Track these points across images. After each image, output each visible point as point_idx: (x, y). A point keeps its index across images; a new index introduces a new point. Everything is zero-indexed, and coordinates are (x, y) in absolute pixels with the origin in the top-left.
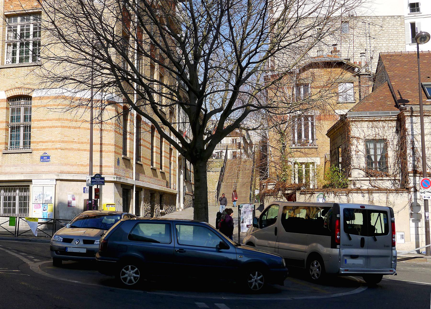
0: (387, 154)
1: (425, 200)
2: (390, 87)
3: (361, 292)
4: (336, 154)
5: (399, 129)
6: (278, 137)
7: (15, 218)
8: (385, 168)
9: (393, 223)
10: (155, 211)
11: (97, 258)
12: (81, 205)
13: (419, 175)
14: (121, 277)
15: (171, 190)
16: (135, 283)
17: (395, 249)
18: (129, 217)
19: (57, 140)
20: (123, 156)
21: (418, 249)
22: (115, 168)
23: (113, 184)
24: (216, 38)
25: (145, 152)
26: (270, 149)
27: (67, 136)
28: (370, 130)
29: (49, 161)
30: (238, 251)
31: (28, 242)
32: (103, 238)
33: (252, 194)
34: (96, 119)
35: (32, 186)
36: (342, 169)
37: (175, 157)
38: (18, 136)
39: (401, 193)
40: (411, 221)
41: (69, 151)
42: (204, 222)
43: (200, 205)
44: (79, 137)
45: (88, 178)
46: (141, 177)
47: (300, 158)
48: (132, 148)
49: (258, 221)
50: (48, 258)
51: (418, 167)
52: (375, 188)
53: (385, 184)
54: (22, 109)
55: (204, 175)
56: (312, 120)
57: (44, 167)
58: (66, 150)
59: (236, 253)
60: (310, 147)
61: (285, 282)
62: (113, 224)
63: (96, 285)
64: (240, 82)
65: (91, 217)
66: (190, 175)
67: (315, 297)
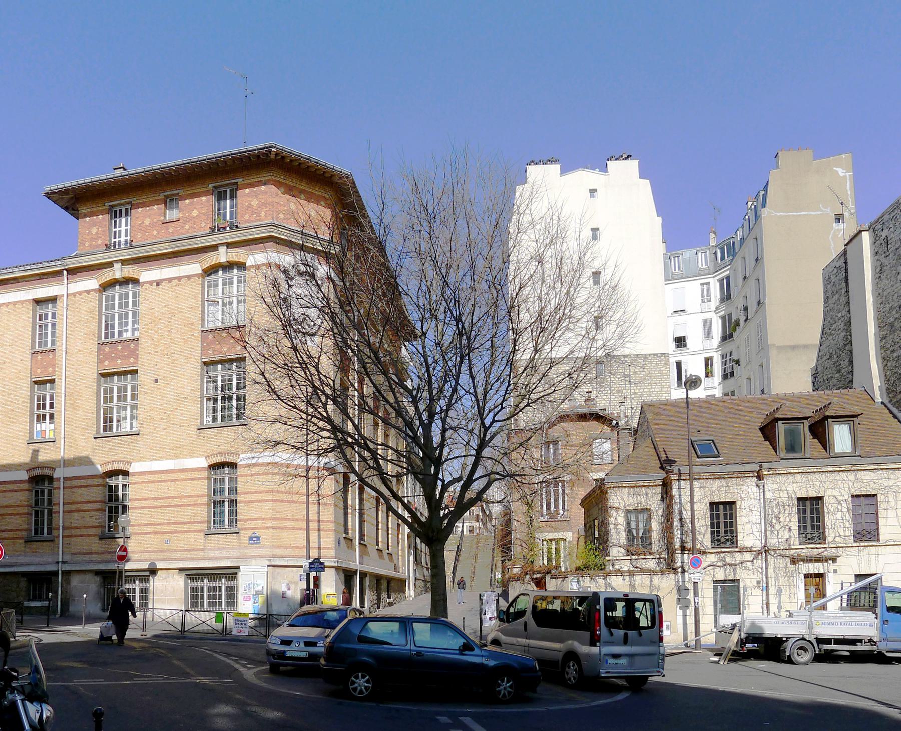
0: (651, 527)
1: (694, 583)
5: (665, 496)
6: (525, 508)
7: (222, 613)
8: (648, 545)
9: (660, 613)
11: (322, 665)
13: (687, 552)
14: (351, 687)
16: (366, 694)
21: (686, 642)
24: (455, 390)
25: (369, 529)
26: (515, 524)
27: (280, 512)
30: (484, 654)
31: (238, 643)
35: (240, 573)
37: (403, 535)
38: (222, 513)
40: (678, 608)
42: (443, 619)
45: (306, 563)
50: (262, 663)
51: (687, 543)
54: (226, 480)
56: (563, 486)
57: (253, 551)
59: (482, 656)
60: (561, 520)
61: (538, 689)
63: (321, 697)
64: (482, 445)
67: (572, 707)
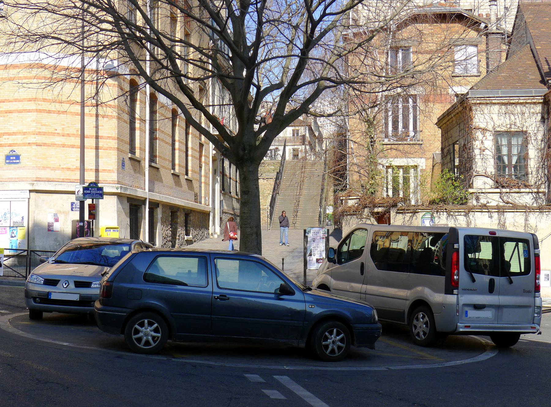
0: (528, 154)
2: (533, 53)
3: (488, 359)
4: (450, 154)
5: (546, 116)
6: (364, 127)
9: (537, 257)
10: (177, 237)
12: (67, 229)
15: (201, 206)
17: (539, 296)
18: (142, 248)
19: (29, 131)
20: (130, 155)
22: (119, 173)
23: (115, 199)
25: (162, 149)
26: (352, 145)
27: (45, 125)
28: (502, 118)
29: (18, 163)
30: (307, 298)
32: (106, 278)
33: (322, 213)
34: (92, 98)
36: (460, 175)
37: (207, 157)
39: (547, 213)
41: (49, 147)
43: (249, 230)
44: (63, 127)
45: (79, 188)
46: (157, 186)
47: (396, 159)
48: (142, 143)
49: (335, 253)
50: (21, 309)
52: (508, 205)
53: (523, 199)
55: (256, 185)
56: (415, 102)
60: (411, 142)
61: (377, 344)
62: (119, 258)
63: (95, 348)
64: (310, 43)
65: (85, 248)
66: (230, 183)
67: (421, 366)
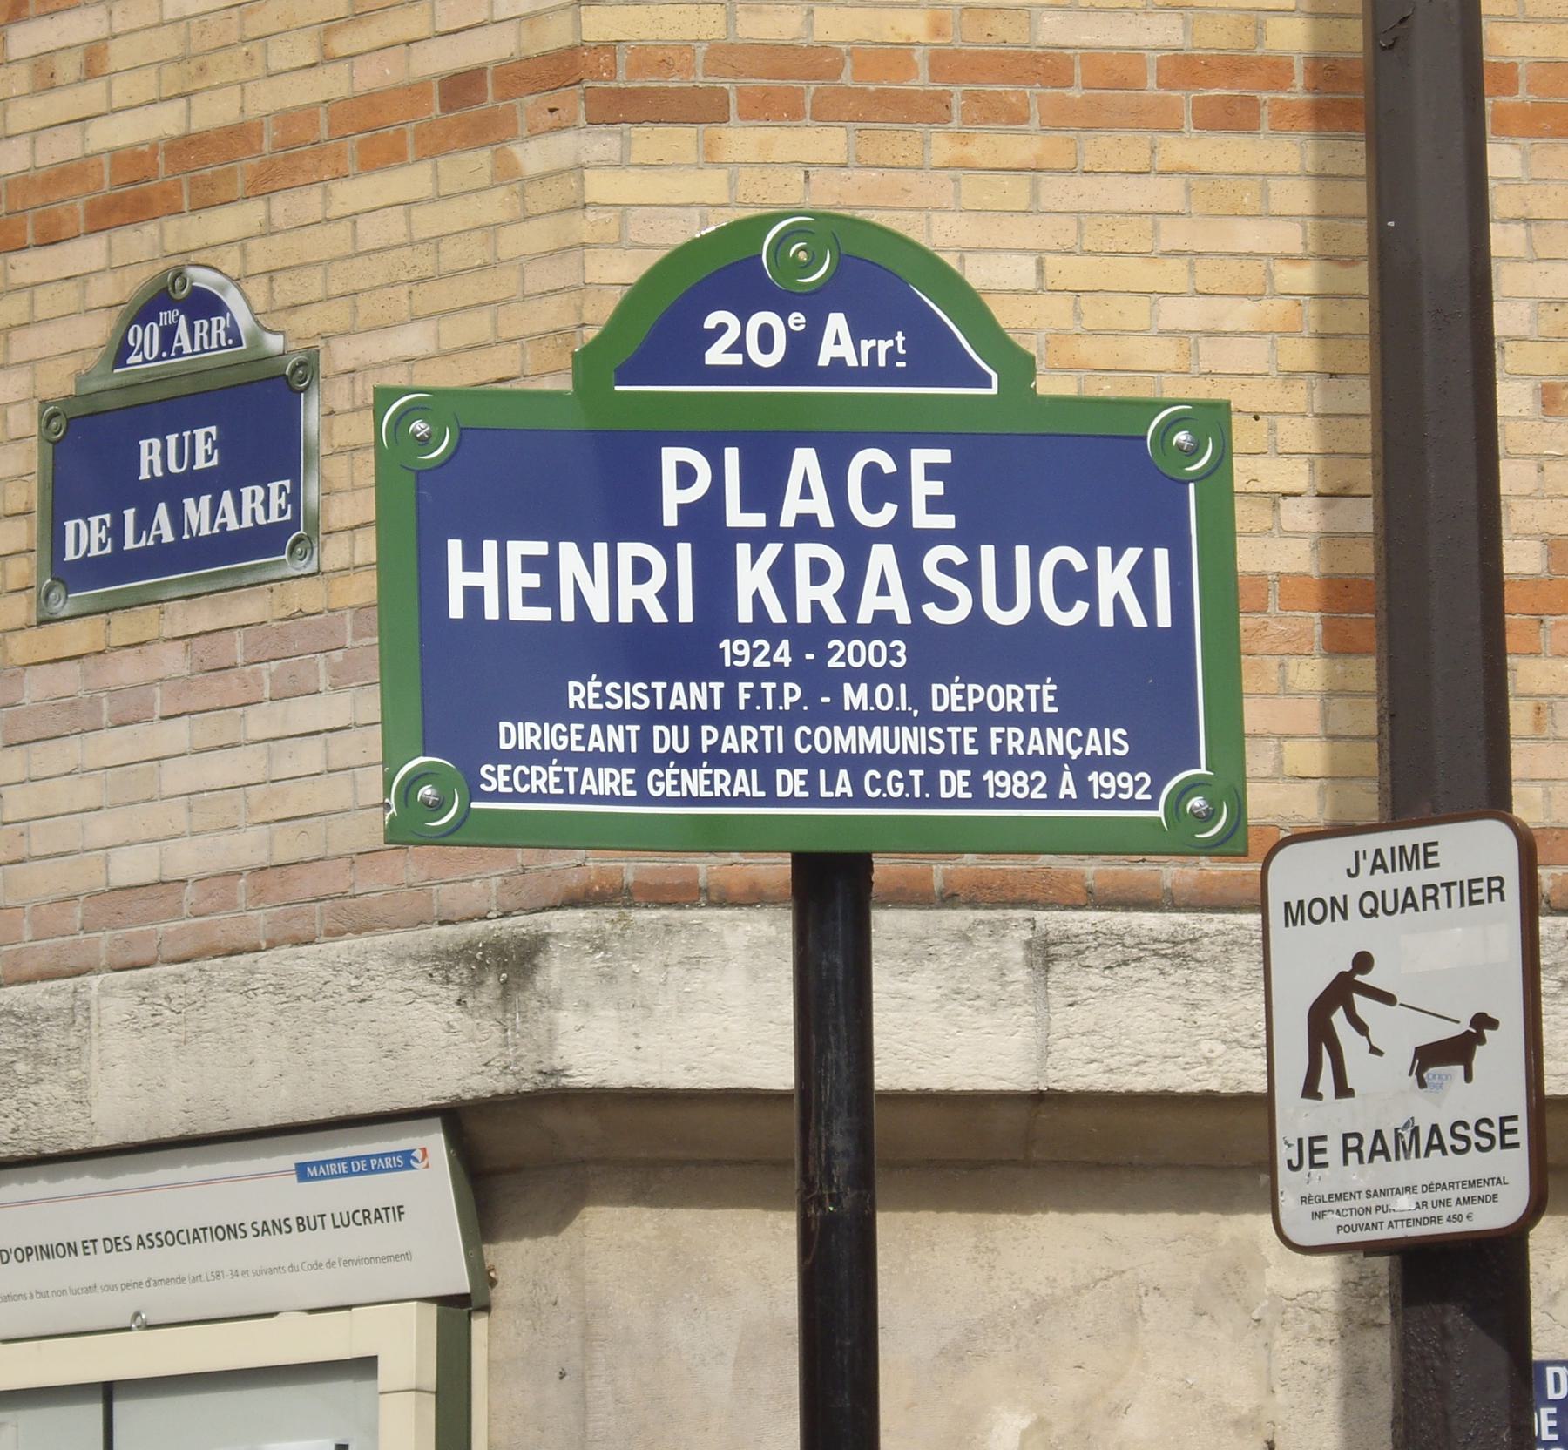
58: (763, 108)
